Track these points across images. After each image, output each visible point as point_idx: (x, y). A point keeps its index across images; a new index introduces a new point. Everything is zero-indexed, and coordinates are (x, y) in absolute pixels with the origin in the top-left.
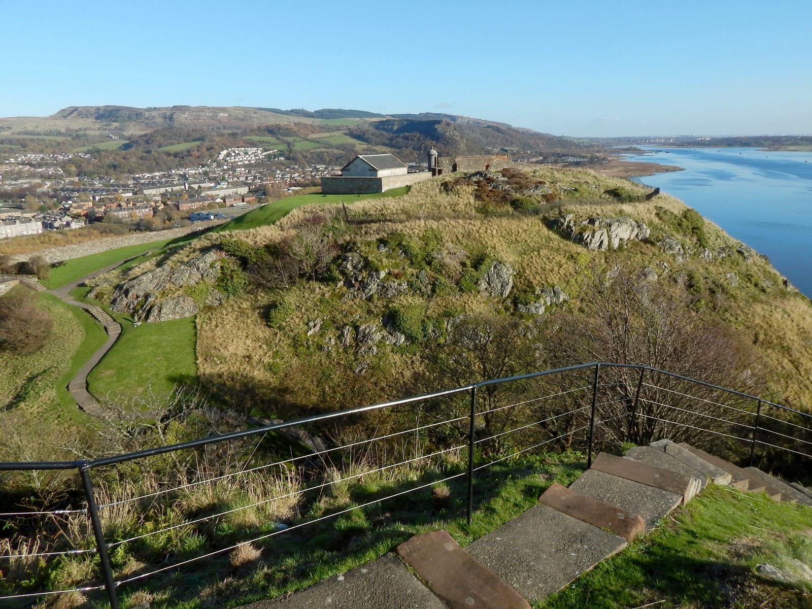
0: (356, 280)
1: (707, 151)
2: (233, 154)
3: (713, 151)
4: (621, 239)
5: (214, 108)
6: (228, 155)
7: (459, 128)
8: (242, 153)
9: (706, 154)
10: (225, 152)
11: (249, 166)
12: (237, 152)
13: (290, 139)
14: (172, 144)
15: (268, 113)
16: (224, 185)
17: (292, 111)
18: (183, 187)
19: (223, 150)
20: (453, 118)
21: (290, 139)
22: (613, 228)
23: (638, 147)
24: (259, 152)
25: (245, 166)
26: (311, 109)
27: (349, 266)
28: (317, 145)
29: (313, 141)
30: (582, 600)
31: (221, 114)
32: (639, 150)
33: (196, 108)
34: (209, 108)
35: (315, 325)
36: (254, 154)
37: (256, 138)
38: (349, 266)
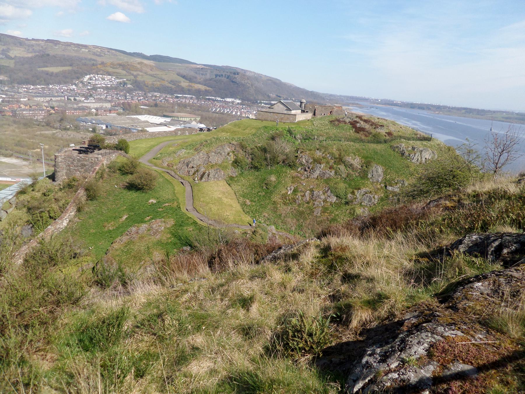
0: (309, 168)
1: (396, 108)
2: (94, 79)
3: (403, 110)
4: (426, 159)
5: (78, 45)
6: (90, 79)
7: (249, 78)
8: (100, 79)
10: (88, 76)
11: (106, 88)
12: (97, 77)
13: (135, 73)
14: (47, 67)
15: (118, 53)
16: (91, 100)
17: (134, 53)
18: (63, 98)
19: (87, 75)
20: (245, 71)
21: (135, 73)
22: (423, 153)
23: (359, 103)
24: (113, 79)
25: (102, 88)
26: (148, 53)
27: (304, 161)
28: (154, 79)
29: (152, 76)
31: (83, 50)
32: (360, 105)
33: (64, 43)
34: (74, 44)
35: (291, 189)
36: (108, 81)
37: (111, 70)
38: (304, 161)
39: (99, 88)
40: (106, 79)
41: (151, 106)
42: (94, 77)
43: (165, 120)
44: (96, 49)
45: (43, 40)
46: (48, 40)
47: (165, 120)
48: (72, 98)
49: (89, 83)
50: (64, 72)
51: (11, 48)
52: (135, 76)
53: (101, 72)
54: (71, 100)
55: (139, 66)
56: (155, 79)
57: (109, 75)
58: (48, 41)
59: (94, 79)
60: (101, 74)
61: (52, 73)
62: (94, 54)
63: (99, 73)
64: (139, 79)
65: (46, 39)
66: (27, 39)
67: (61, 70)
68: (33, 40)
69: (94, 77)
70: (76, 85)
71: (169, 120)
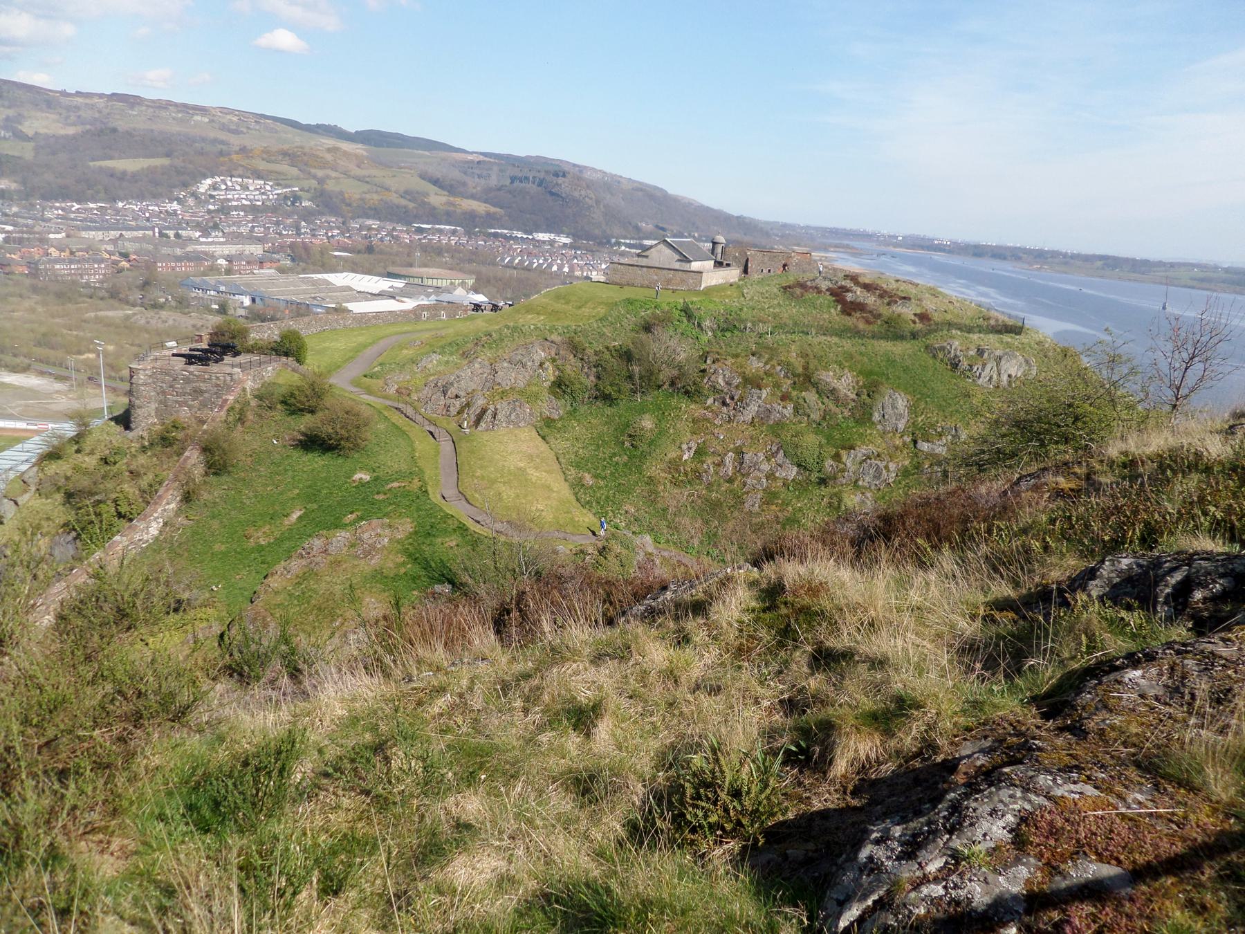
1: (938, 257)
2: (223, 187)
3: (956, 261)
4: (1009, 376)
5: (185, 106)
6: (214, 187)
7: (590, 185)
8: (238, 188)
9: (369, 272)
10: (209, 181)
11: (252, 209)
12: (229, 184)
13: (320, 173)
14: (111, 158)
15: (279, 126)
16: (216, 236)
17: (318, 126)
18: (150, 233)
19: (205, 177)
20: (582, 169)
21: (320, 173)
22: (1003, 362)
23: (852, 243)
24: (268, 188)
25: (243, 208)
26: (351, 127)
27: (720, 381)
28: (366, 187)
29: (359, 179)
30: (1238, 880)
31: (198, 118)
32: (853, 248)
33: (153, 101)
34: (176, 105)
36: (256, 191)
37: (262, 166)
38: (720, 381)
39: (236, 208)
40: (251, 188)
41: (359, 252)
42: (224, 182)
43: (390, 284)
44: (228, 117)
45: (101, 96)
46: (114, 94)
47: (390, 284)
48: (171, 233)
49: (212, 197)
50: (152, 170)
51: (26, 113)
52: (321, 181)
53: (240, 171)
54: (167, 236)
55: (329, 157)
56: (368, 186)
57: (259, 178)
58: (114, 96)
59: (223, 187)
60: (240, 176)
61: (124, 173)
62: (224, 128)
63: (234, 173)
64: (330, 186)
65: (108, 92)
66: (64, 93)
67: (145, 166)
68: (78, 94)
69: (224, 182)
70: (179, 201)
71: (401, 285)
